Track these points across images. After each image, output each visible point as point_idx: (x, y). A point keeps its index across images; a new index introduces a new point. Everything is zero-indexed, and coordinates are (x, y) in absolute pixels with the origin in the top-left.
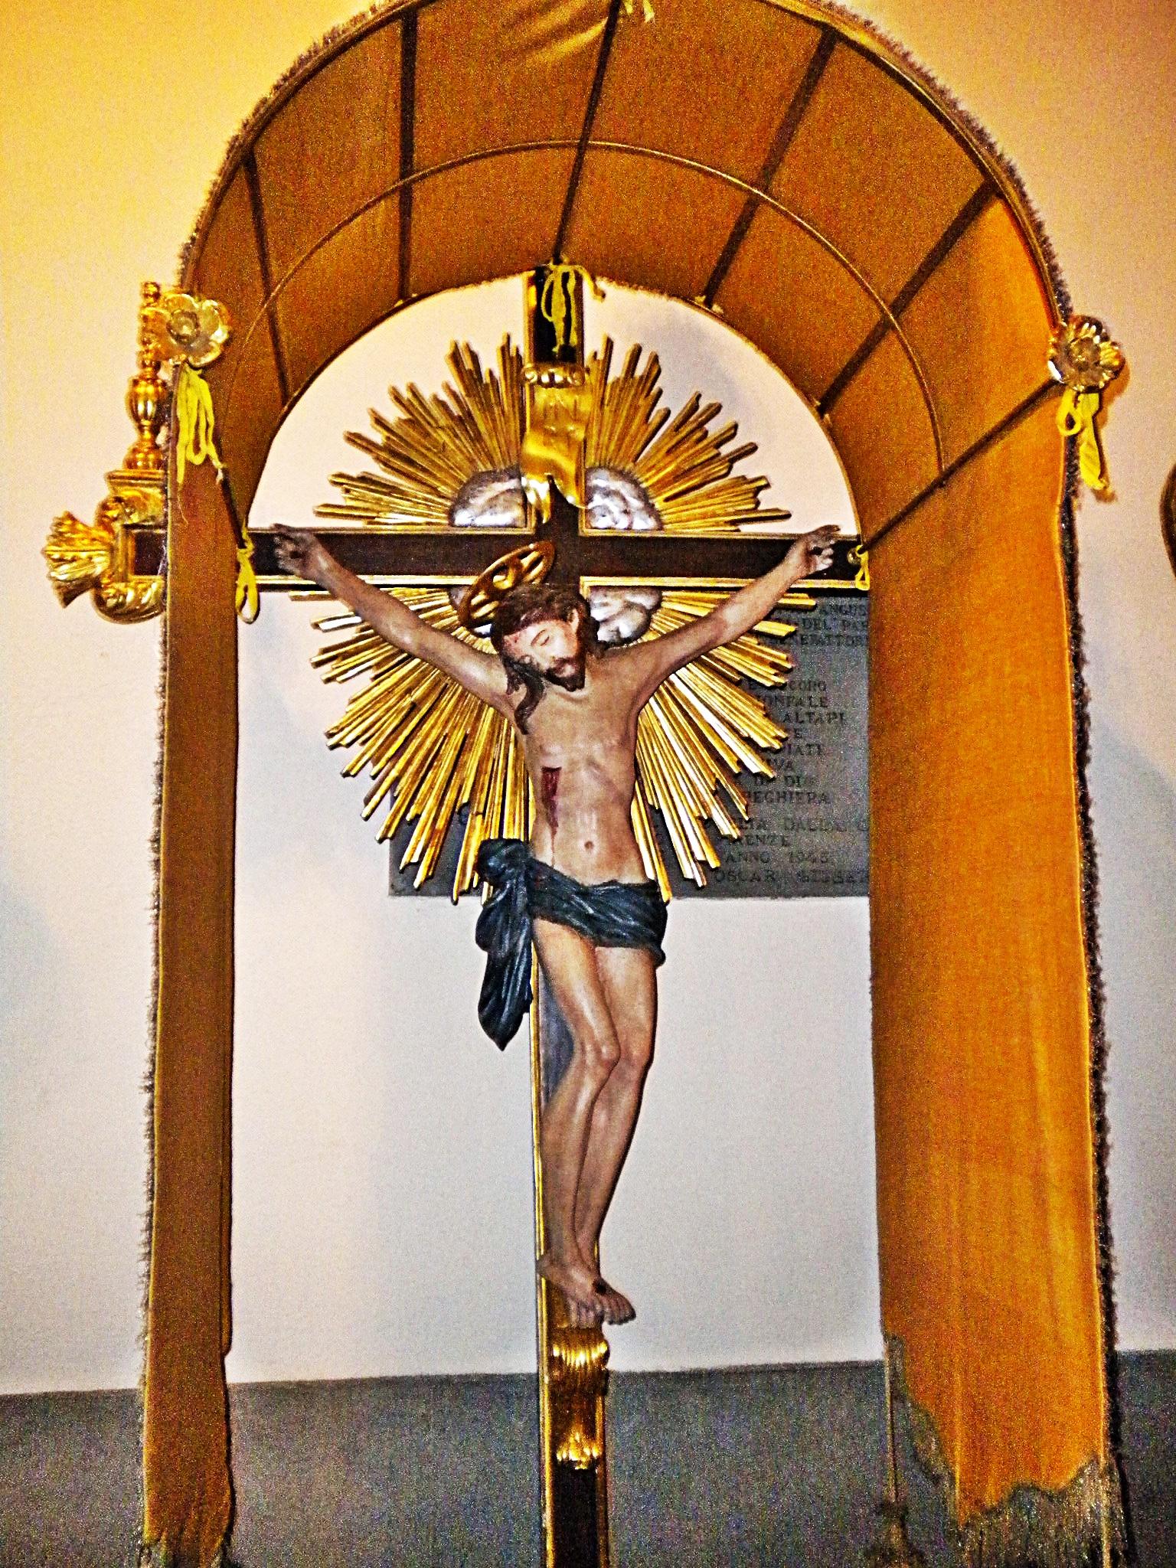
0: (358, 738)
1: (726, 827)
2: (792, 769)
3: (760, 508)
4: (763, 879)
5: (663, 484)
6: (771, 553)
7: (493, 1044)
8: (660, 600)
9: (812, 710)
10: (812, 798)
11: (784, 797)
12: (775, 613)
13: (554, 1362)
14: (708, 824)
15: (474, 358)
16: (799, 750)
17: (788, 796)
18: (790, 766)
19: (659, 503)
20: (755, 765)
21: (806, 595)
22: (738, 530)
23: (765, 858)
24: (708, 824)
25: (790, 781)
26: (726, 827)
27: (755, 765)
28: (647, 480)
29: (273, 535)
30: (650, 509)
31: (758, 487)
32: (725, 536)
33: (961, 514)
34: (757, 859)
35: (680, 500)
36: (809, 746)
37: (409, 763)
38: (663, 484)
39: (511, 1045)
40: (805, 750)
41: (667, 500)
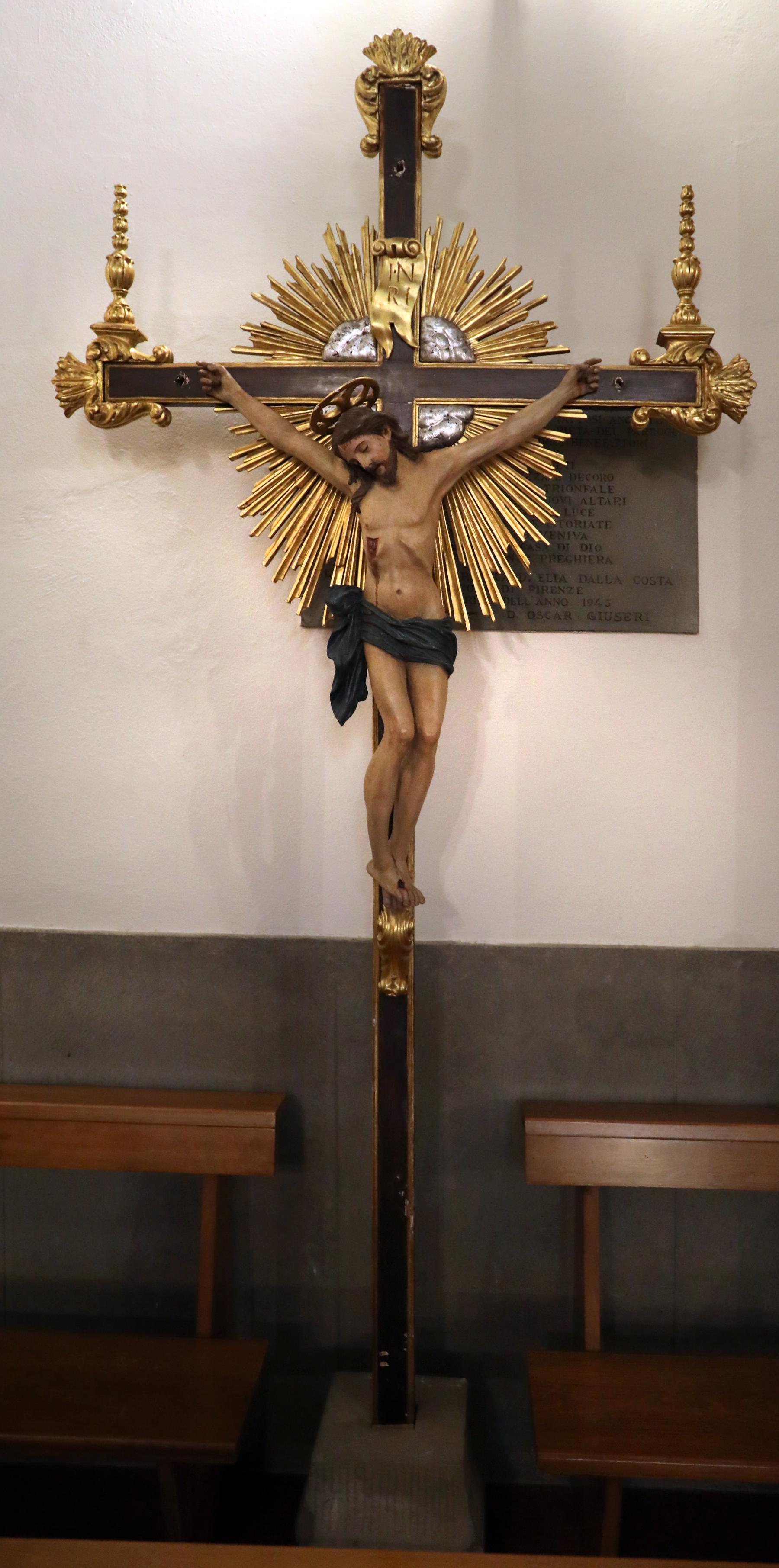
0: (260, 510)
1: (512, 580)
2: (586, 539)
3: (548, 345)
4: (562, 618)
5: (477, 326)
6: (553, 376)
7: (336, 721)
8: (473, 414)
9: (602, 495)
10: (600, 559)
11: (580, 559)
12: (558, 424)
13: (378, 929)
14: (500, 579)
15: (342, 234)
16: (592, 525)
17: (583, 558)
18: (584, 537)
19: (473, 340)
20: (538, 536)
21: (581, 411)
22: (531, 363)
23: (564, 603)
24: (500, 579)
25: (584, 547)
26: (512, 580)
27: (538, 536)
28: (465, 324)
29: (198, 369)
30: (466, 346)
31: (541, 330)
32: (519, 367)
33: (157, 445)
34: (559, 604)
35: (489, 339)
36: (600, 522)
37: (293, 528)
38: (477, 326)
39: (346, 723)
40: (596, 525)
41: (479, 339)
